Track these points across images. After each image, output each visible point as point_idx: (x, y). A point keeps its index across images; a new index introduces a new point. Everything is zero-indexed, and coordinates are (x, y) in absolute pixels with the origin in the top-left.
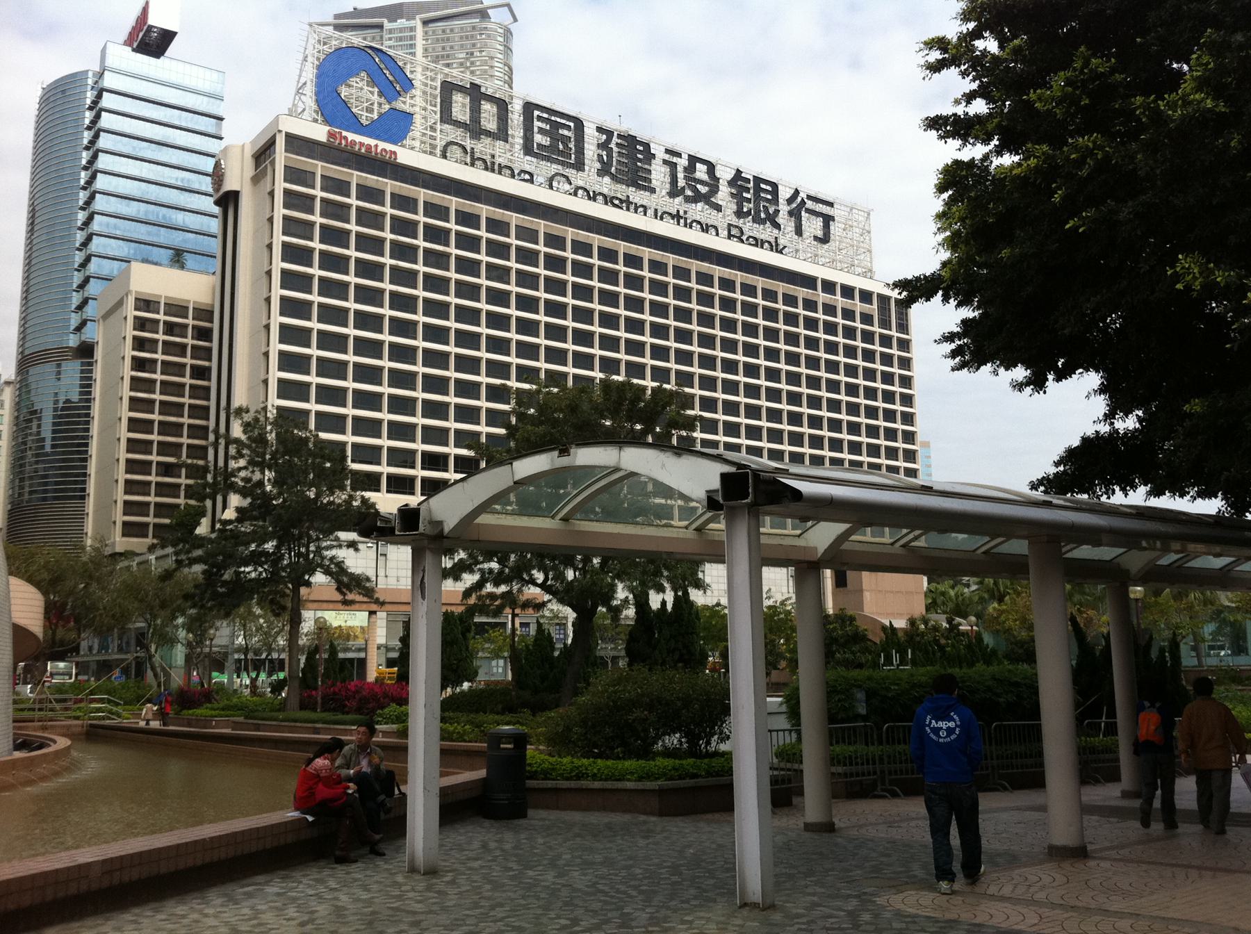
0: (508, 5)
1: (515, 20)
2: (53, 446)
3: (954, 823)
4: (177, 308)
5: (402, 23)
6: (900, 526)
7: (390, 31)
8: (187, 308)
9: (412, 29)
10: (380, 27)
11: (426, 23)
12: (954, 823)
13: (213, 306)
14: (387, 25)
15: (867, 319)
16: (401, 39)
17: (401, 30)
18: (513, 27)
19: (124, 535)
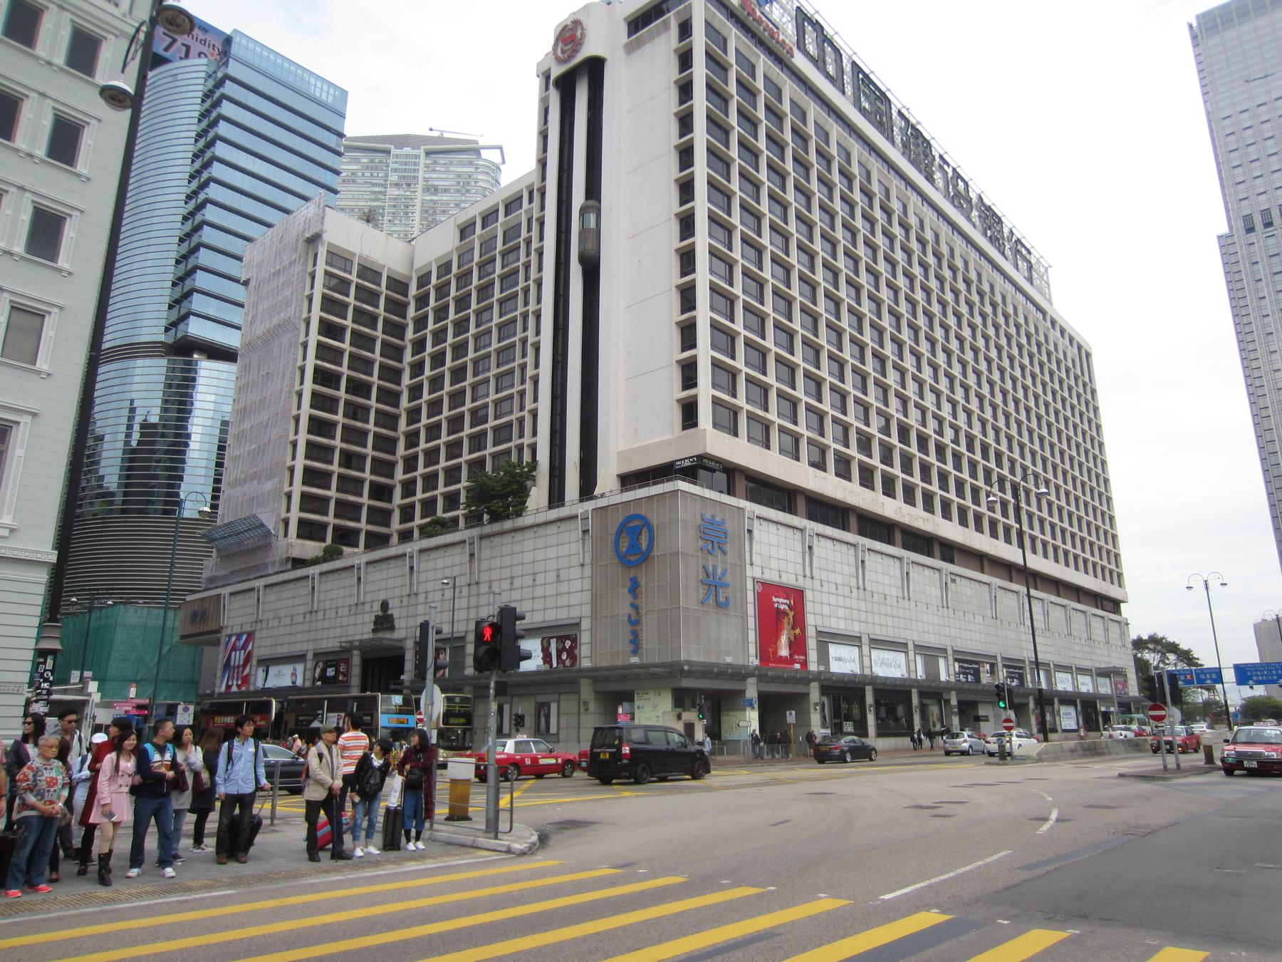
0: (501, 148)
1: (504, 162)
2: (139, 443)
3: (847, 902)
4: (369, 272)
5: (407, 150)
6: (782, 624)
7: (397, 156)
8: (380, 274)
9: (417, 157)
10: (388, 152)
11: (428, 153)
12: (847, 902)
13: (411, 278)
14: (394, 151)
15: (429, 505)
16: (406, 164)
17: (407, 156)
18: (502, 167)
19: (299, 536)
